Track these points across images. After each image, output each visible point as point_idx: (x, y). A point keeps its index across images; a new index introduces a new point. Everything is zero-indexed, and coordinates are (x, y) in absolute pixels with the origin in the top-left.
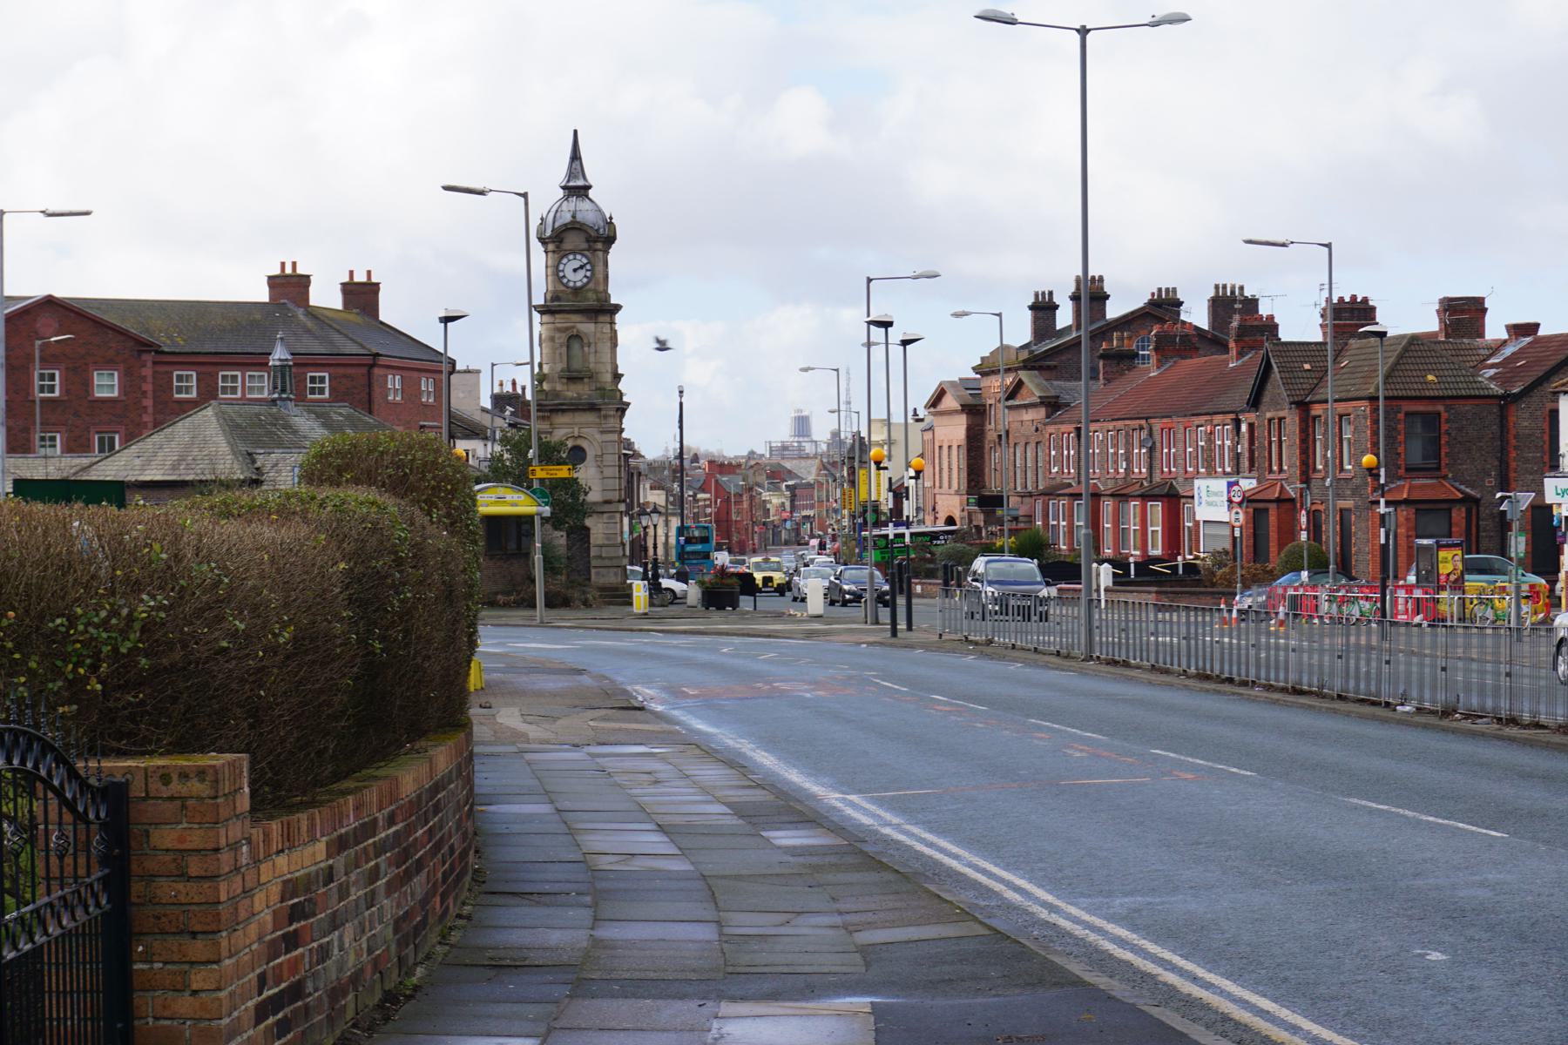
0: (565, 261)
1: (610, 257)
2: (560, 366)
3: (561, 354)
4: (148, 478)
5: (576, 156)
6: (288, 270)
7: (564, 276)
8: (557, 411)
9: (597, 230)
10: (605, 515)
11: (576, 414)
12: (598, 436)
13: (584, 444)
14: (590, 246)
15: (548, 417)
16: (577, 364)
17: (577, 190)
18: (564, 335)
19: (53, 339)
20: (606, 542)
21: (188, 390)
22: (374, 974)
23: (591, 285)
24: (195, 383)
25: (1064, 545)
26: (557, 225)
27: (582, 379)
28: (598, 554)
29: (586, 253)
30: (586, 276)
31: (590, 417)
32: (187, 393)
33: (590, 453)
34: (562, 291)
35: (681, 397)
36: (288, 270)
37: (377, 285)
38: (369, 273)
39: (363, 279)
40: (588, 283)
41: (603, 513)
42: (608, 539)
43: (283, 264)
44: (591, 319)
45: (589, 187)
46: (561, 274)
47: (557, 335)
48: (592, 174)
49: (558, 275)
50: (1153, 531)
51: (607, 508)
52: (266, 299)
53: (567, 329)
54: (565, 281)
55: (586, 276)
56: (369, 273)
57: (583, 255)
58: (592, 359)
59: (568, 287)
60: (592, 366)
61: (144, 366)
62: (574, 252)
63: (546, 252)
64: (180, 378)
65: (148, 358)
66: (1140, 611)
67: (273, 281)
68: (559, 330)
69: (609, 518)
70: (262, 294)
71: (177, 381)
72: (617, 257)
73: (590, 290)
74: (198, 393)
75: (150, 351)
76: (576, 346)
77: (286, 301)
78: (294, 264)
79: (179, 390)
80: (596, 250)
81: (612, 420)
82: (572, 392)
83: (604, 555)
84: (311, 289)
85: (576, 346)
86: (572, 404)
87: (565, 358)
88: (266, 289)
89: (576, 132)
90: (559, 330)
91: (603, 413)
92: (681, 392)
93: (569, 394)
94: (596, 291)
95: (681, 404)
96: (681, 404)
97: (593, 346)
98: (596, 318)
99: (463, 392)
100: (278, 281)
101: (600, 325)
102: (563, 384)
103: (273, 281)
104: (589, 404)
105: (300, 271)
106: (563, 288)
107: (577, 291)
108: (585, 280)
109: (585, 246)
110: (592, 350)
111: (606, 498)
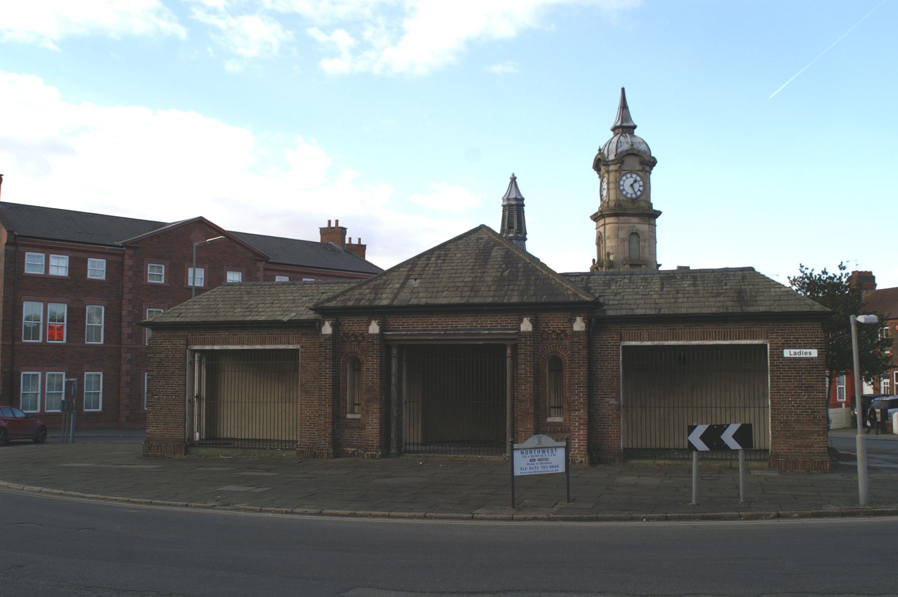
1: (652, 176)
4: (444, 301)
5: (624, 106)
7: (624, 190)
14: (643, 168)
17: (625, 127)
19: (207, 240)
23: (643, 197)
26: (619, 151)
29: (640, 173)
36: (333, 225)
37: (364, 246)
38: (360, 239)
39: (357, 243)
40: (641, 195)
43: (330, 222)
45: (635, 127)
46: (622, 188)
48: (635, 119)
49: (619, 188)
50: (839, 388)
54: (624, 193)
55: (640, 186)
56: (360, 239)
57: (638, 175)
61: (259, 270)
62: (631, 172)
65: (261, 265)
67: (323, 231)
70: (317, 238)
72: (655, 175)
73: (642, 200)
75: (263, 261)
76: (634, 238)
78: (337, 221)
88: (319, 236)
89: (623, 90)
103: (323, 231)
108: (622, 188)
109: (639, 167)
110: (647, 244)
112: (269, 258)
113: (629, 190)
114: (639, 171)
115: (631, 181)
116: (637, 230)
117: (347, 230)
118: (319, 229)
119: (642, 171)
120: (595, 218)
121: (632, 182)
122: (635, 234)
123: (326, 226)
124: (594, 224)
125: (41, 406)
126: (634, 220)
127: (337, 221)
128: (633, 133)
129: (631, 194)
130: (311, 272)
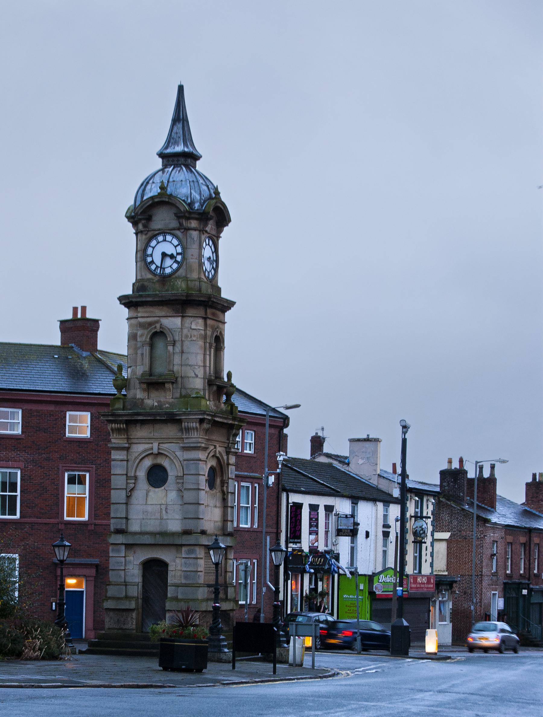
0: (153, 243)
2: (140, 370)
3: (142, 354)
8: (136, 422)
9: (191, 205)
10: (184, 549)
11: (157, 426)
12: (179, 453)
13: (166, 463)
14: (181, 224)
15: (126, 431)
16: (160, 369)
18: (146, 332)
20: (184, 581)
23: (181, 272)
25: (258, 655)
26: (145, 198)
27: (163, 384)
28: (175, 595)
29: (178, 233)
30: (152, 262)
31: (170, 431)
33: (172, 474)
34: (149, 280)
35: (404, 433)
41: (182, 545)
42: (186, 577)
44: (177, 312)
46: (149, 259)
49: (145, 260)
51: (185, 540)
52: (58, 342)
53: (150, 324)
54: (153, 267)
57: (174, 236)
58: (177, 360)
59: (155, 275)
60: (176, 368)
62: (164, 233)
63: (137, 234)
68: (142, 326)
69: (189, 552)
73: (179, 277)
77: (73, 345)
83: (180, 597)
84: (100, 333)
85: (160, 344)
87: (147, 361)
88: (59, 334)
89: (181, 89)
90: (142, 326)
92: (405, 428)
93: (149, 402)
94: (186, 279)
95: (404, 441)
96: (404, 441)
97: (178, 345)
98: (183, 311)
100: (67, 324)
101: (188, 321)
102: (144, 390)
104: (167, 414)
105: (89, 316)
106: (150, 276)
107: (164, 279)
108: (149, 259)
109: (174, 224)
110: (178, 348)
111: (188, 528)
113: (157, 259)
114: (174, 229)
115: (170, 249)
117: (100, 322)
118: (59, 323)
119: (179, 229)
120: (126, 301)
123: (70, 316)
124: (125, 312)
128: (195, 167)
129: (157, 267)
130: (49, 399)
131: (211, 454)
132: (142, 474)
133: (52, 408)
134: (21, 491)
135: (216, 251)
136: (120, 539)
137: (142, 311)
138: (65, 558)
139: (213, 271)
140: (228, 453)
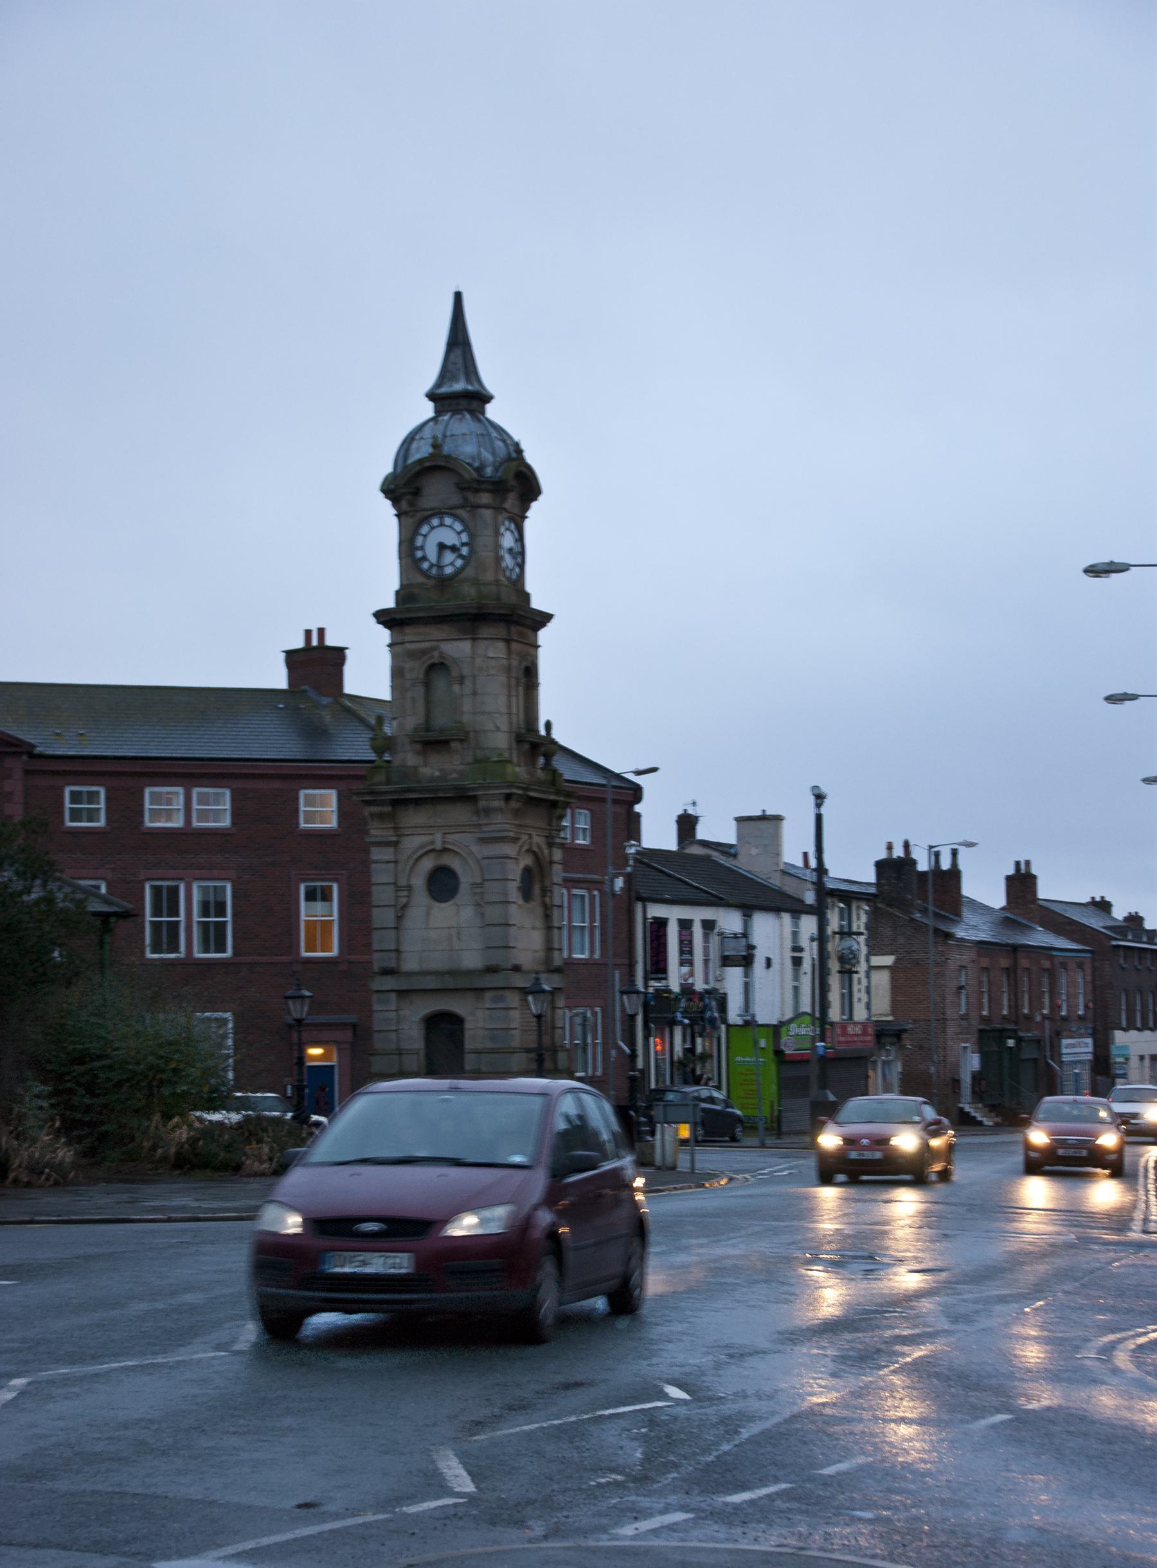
0: (425, 529)
2: (412, 722)
3: (413, 699)
6: (315, 642)
8: (406, 802)
12: (475, 848)
13: (455, 864)
16: (441, 720)
20: (490, 1045)
21: (92, 815)
22: (945, 1523)
24: (102, 805)
27: (446, 743)
29: (461, 512)
31: (460, 814)
32: (90, 820)
33: (466, 879)
34: (420, 585)
40: (463, 568)
45: (486, 398)
46: (419, 554)
47: (408, 665)
48: (490, 375)
54: (425, 565)
57: (456, 517)
58: (467, 705)
60: (466, 718)
62: (440, 513)
64: (76, 797)
65: (17, 766)
66: (1061, 1220)
67: (292, 657)
68: (413, 655)
70: (277, 678)
71: (72, 802)
72: (536, 510)
74: (108, 819)
75: (20, 754)
79: (76, 815)
80: (477, 507)
81: (499, 818)
82: (432, 768)
86: (427, 790)
89: (458, 297)
90: (413, 655)
91: (482, 804)
92: (820, 798)
93: (426, 771)
95: (819, 818)
96: (819, 818)
97: (468, 683)
99: (757, 847)
101: (482, 645)
104: (456, 788)
105: (330, 642)
106: (420, 579)
108: (419, 554)
109: (456, 499)
110: (468, 687)
112: (33, 746)
113: (432, 553)
116: (441, 657)
118: (284, 654)
119: (462, 507)
121: (449, 543)
122: (438, 667)
123: (299, 643)
125: (594, 908)
126: (435, 632)
127: (321, 631)
128: (483, 413)
131: (526, 847)
132: (419, 882)
133: (277, 785)
134: (234, 915)
135: (520, 539)
136: (389, 983)
137: (410, 633)
138: (304, 1016)
139: (517, 570)
140: (550, 845)
